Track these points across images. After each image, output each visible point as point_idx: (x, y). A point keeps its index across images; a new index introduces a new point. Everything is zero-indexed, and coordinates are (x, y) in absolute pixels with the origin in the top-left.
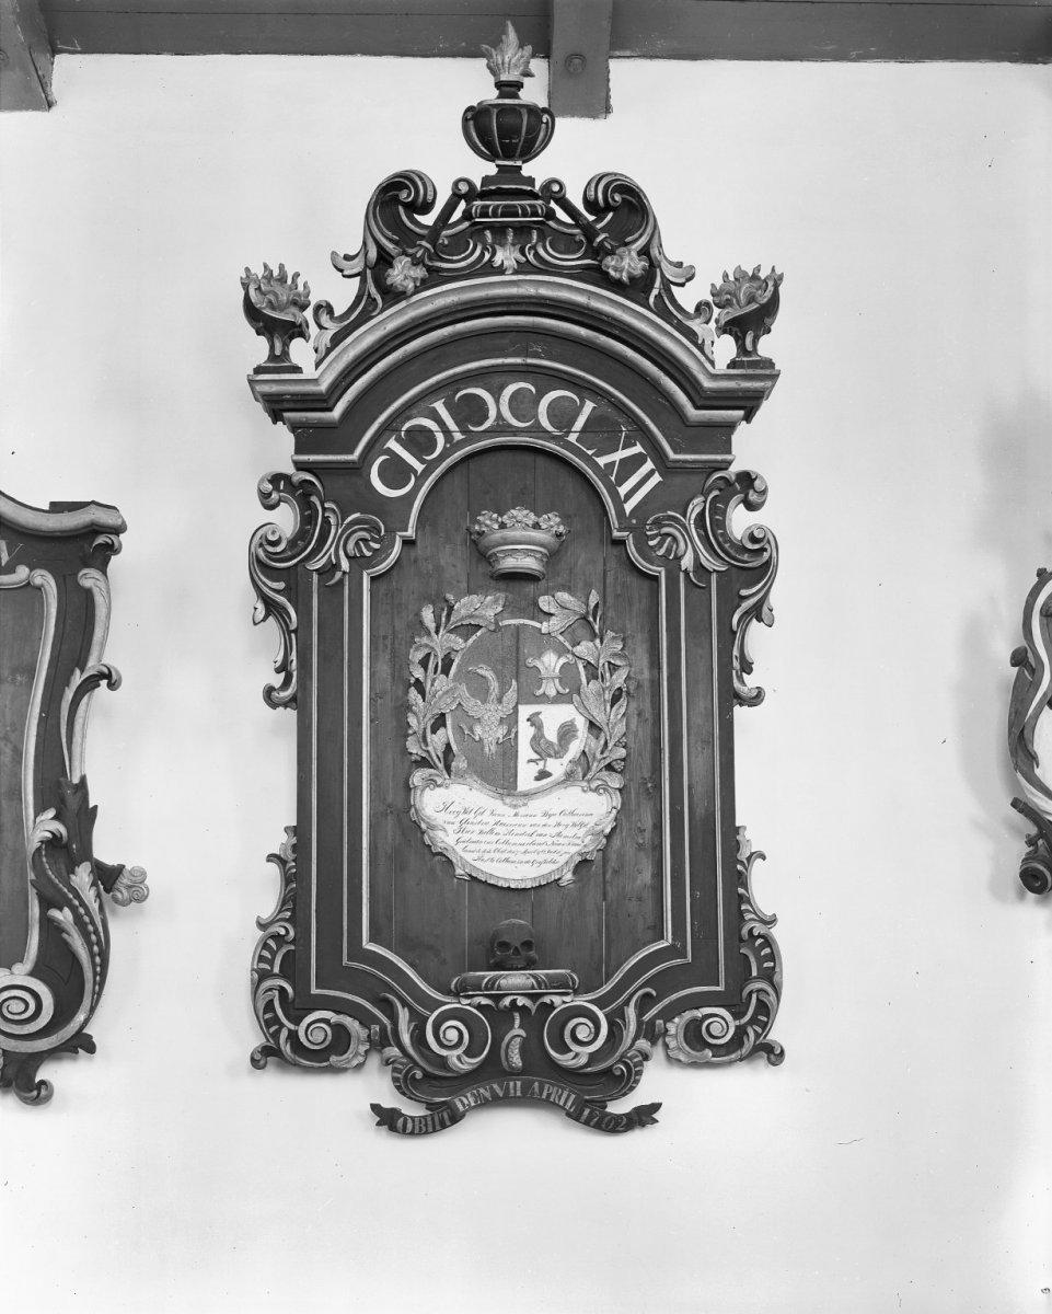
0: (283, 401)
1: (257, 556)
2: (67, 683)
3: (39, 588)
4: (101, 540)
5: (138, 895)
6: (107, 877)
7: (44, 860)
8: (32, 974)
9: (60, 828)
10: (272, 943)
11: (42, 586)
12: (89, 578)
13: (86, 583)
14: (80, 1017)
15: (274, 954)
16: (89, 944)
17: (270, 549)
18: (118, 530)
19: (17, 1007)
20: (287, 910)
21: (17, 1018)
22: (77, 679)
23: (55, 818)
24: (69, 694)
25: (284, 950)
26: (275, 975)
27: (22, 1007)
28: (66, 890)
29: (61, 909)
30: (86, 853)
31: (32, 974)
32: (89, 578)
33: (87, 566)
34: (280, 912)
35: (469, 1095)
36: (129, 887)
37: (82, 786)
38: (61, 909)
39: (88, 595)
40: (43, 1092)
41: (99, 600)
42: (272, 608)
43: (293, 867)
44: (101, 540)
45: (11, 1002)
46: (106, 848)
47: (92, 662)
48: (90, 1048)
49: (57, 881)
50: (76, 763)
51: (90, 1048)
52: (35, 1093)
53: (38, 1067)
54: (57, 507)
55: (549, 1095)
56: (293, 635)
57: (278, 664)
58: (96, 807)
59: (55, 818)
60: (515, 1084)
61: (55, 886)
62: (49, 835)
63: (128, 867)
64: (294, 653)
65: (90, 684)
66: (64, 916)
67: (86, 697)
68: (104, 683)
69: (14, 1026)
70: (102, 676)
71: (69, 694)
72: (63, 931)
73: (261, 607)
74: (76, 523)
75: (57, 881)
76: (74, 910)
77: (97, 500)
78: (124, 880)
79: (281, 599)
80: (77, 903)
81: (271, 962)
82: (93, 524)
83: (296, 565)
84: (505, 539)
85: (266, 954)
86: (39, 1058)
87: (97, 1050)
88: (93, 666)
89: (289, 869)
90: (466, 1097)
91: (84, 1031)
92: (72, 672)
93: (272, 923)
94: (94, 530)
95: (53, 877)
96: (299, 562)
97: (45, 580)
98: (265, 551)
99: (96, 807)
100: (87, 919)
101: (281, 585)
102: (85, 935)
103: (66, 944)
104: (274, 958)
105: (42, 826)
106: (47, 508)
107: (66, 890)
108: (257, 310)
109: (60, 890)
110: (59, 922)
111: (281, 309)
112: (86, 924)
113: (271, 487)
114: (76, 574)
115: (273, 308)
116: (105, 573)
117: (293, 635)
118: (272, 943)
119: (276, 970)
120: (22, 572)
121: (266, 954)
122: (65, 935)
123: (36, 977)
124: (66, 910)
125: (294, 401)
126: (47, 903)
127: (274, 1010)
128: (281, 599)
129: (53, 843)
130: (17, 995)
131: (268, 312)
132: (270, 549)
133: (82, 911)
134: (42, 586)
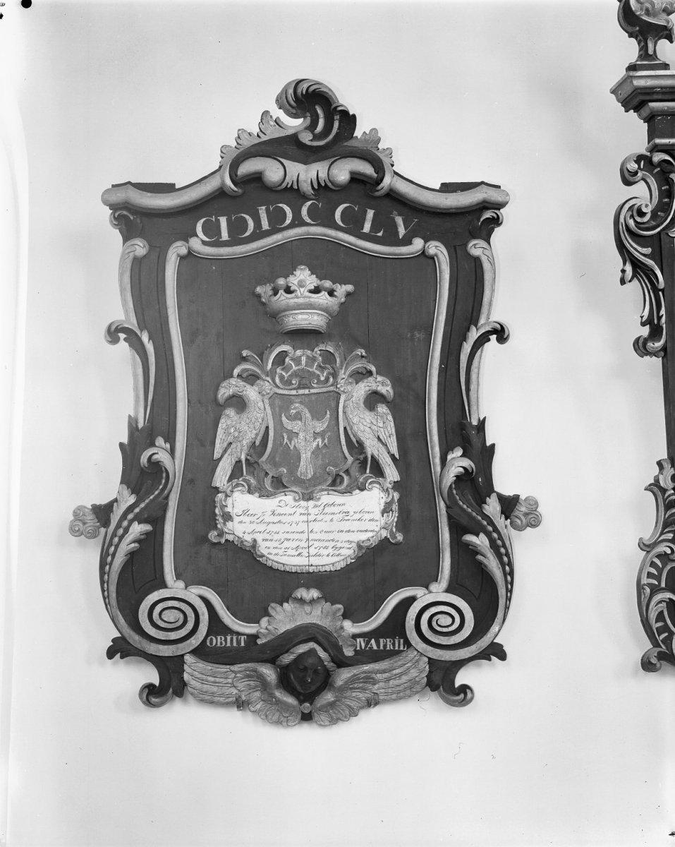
0: (653, 93)
1: (626, 226)
2: (465, 339)
3: (432, 258)
4: (488, 214)
5: (533, 520)
6: (509, 505)
7: (455, 492)
8: (448, 590)
9: (467, 463)
10: (658, 562)
11: (436, 255)
12: (476, 248)
13: (475, 252)
14: (495, 628)
15: (660, 571)
16: (503, 564)
17: (639, 219)
18: (500, 206)
19: (445, 620)
20: (669, 532)
21: (445, 630)
22: (474, 335)
23: (463, 455)
24: (467, 347)
25: (669, 567)
26: (663, 589)
27: (449, 621)
28: (480, 518)
29: (477, 535)
30: (490, 489)
31: (448, 590)
32: (476, 248)
33: (474, 237)
34: (662, 533)
35: (219, 638)
36: (526, 514)
37: (482, 424)
38: (477, 535)
39: (477, 261)
40: (469, 695)
41: (486, 266)
42: (638, 266)
43: (672, 495)
44: (488, 214)
45: (439, 616)
46: (506, 479)
47: (482, 321)
48: (502, 656)
49: (470, 510)
50: (474, 408)
51: (502, 656)
52: (462, 696)
53: (459, 669)
54: (447, 188)
55: (385, 646)
56: (660, 293)
57: (644, 319)
58: (493, 445)
59: (463, 455)
60: (399, 648)
61: (469, 515)
62: (462, 470)
63: (523, 497)
64: (663, 308)
65: (483, 339)
66: (481, 541)
67: (480, 350)
68: (493, 337)
69: (442, 637)
70: (494, 331)
71: (467, 347)
72: (477, 553)
73: (629, 268)
74: (471, 201)
75: (470, 510)
76: (488, 535)
77: (486, 181)
78: (523, 508)
79: (650, 262)
80: (490, 528)
81: (658, 578)
82: (484, 202)
83: (659, 233)
84: (288, 306)
85: (653, 571)
86: (461, 664)
87: (508, 656)
88: (487, 320)
89: (669, 496)
90: (217, 639)
91: (495, 641)
92: (468, 329)
93: (656, 544)
94: (485, 205)
95: (465, 507)
96: (661, 230)
97: (437, 249)
98: (635, 221)
99: (493, 445)
100: (499, 542)
101: (648, 251)
102: (499, 556)
103: (480, 563)
104: (660, 574)
105: (458, 462)
106: (438, 187)
107: (480, 518)
108: (636, 16)
109: (474, 518)
110: (475, 546)
111: (655, 15)
112: (498, 546)
113: (636, 166)
114: (466, 245)
115: (648, 13)
116: (489, 243)
117: (660, 293)
118: (658, 562)
119: (663, 585)
120: (418, 244)
121: (653, 571)
122: (479, 557)
123: (450, 593)
124: (482, 535)
125: (663, 93)
126: (458, 529)
127: (664, 621)
128: (650, 262)
129: (464, 478)
130: (443, 610)
131: (645, 18)
132: (639, 219)
133: (495, 535)
134: (436, 255)
